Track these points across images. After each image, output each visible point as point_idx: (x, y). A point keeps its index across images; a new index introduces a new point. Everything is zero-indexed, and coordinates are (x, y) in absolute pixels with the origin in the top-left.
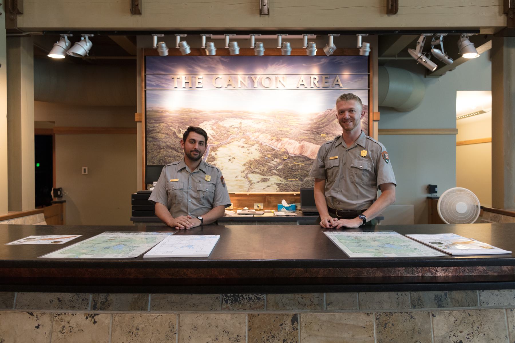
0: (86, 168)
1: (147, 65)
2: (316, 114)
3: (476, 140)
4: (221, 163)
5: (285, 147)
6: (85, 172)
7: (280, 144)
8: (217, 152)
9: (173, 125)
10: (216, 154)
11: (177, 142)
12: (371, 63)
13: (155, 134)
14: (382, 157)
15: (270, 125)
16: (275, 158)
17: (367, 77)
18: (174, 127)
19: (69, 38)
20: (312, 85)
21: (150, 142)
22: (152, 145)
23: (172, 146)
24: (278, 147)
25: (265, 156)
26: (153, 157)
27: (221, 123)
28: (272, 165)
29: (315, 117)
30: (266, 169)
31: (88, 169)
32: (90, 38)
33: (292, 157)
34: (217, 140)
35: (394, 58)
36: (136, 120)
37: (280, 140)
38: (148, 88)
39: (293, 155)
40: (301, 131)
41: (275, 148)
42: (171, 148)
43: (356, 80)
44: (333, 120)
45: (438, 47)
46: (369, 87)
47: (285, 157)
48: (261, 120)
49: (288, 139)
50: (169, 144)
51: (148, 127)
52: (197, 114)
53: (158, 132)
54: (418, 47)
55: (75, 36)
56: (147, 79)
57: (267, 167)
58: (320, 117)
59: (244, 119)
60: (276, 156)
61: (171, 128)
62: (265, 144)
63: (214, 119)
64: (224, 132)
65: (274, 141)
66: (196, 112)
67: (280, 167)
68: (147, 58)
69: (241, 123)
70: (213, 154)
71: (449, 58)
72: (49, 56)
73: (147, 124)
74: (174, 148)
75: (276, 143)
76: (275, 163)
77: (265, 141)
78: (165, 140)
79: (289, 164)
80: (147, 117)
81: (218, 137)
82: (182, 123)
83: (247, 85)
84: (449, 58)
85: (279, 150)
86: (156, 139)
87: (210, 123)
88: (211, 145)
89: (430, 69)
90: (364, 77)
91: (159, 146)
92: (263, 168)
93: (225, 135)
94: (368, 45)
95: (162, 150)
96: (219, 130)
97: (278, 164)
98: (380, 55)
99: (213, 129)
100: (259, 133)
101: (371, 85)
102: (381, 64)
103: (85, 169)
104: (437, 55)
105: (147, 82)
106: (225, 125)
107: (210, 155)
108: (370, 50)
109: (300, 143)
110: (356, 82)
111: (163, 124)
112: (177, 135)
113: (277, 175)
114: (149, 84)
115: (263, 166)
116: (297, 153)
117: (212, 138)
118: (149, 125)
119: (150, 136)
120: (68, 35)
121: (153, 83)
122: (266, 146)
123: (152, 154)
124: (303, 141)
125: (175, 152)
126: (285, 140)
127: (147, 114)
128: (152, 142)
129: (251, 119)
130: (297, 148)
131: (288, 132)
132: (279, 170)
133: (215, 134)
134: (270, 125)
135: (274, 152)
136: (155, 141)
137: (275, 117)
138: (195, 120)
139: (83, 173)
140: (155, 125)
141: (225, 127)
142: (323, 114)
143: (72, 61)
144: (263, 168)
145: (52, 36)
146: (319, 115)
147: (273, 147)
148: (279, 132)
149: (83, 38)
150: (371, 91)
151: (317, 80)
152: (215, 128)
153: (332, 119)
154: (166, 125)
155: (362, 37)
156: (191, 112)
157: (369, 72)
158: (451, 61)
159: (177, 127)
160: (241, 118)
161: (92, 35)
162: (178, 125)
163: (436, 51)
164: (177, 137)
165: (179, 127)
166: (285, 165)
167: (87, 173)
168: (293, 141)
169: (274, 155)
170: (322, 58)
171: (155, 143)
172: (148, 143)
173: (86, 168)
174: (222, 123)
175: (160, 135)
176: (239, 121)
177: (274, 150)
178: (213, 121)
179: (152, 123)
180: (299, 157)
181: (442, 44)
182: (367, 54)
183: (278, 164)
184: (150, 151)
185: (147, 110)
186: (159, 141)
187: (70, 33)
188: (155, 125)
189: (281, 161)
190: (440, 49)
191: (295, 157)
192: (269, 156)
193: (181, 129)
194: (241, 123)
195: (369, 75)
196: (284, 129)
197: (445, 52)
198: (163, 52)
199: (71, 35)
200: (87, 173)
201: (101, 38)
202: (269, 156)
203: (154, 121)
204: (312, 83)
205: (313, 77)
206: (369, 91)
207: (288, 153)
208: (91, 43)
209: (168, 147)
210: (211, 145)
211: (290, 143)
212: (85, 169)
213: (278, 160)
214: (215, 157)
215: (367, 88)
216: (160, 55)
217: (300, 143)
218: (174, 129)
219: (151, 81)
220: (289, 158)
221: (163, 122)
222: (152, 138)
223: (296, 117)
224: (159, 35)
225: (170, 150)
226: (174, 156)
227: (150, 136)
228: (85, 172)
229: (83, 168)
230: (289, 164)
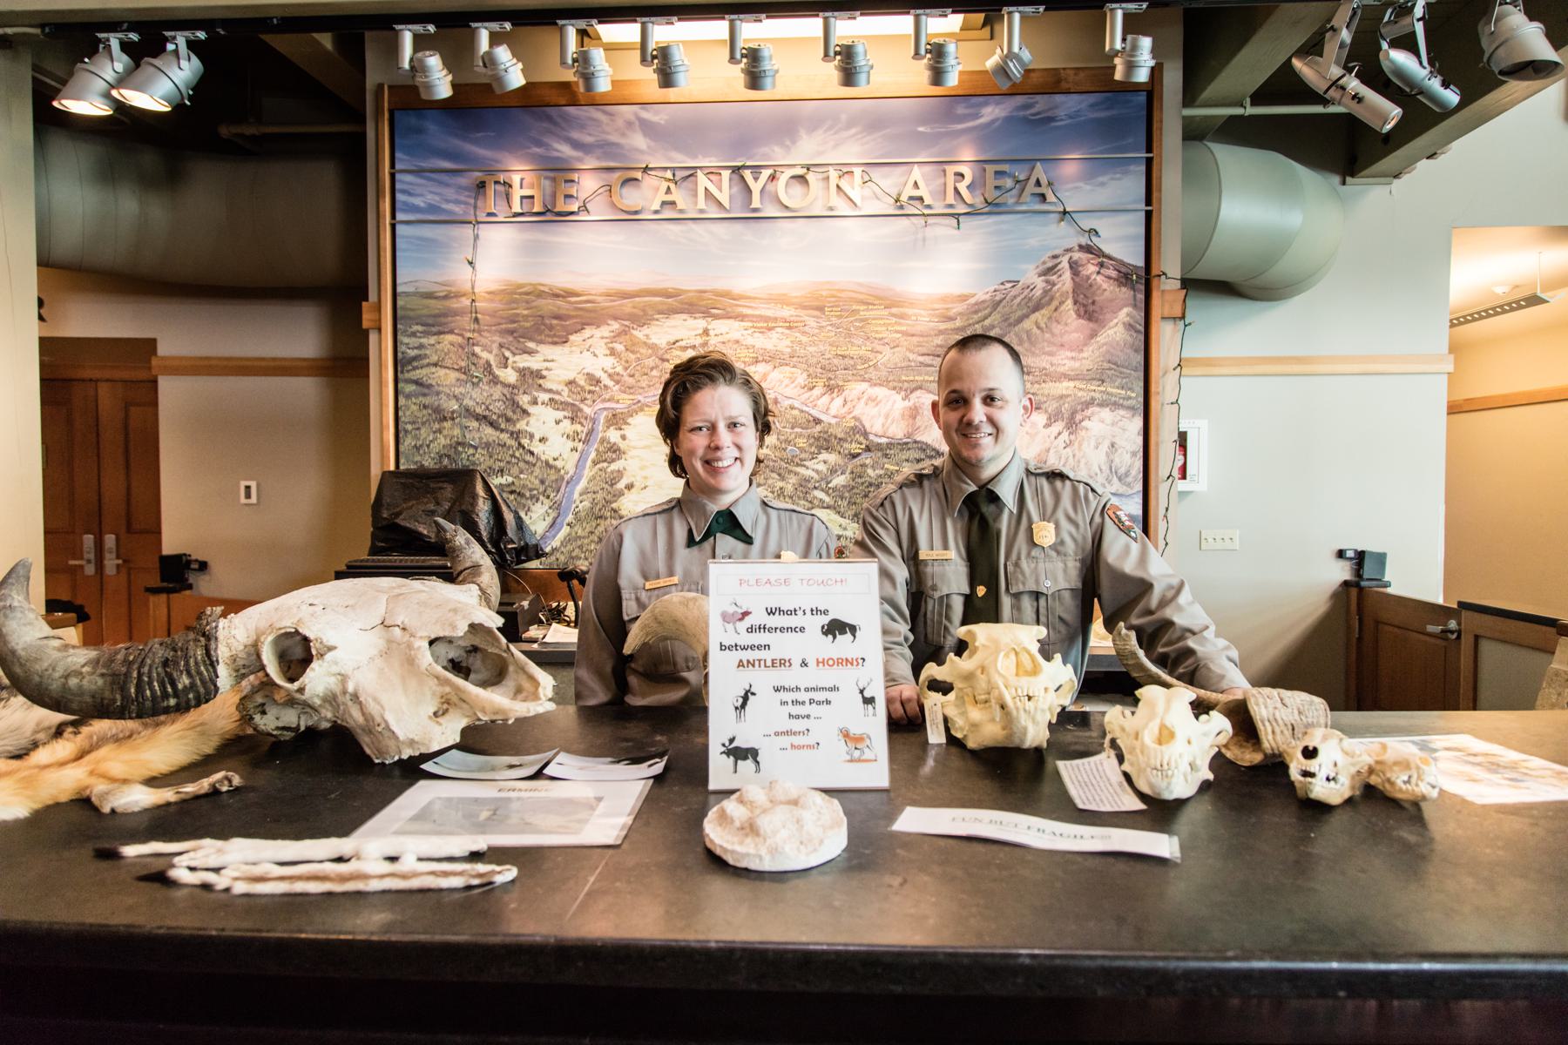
0: (253, 484)
1: (397, 141)
2: (963, 298)
3: (1504, 397)
4: (642, 468)
5: (856, 413)
6: (248, 496)
7: (838, 401)
8: (628, 431)
9: (483, 341)
10: (624, 437)
11: (496, 396)
12: (1155, 125)
13: (424, 371)
14: (1109, 523)
15: (804, 339)
16: (820, 448)
17: (1143, 168)
18: (485, 348)
19: (126, 47)
20: (951, 198)
21: (408, 397)
22: (415, 408)
23: (478, 410)
24: (833, 411)
25: (788, 442)
26: (417, 448)
27: (640, 334)
28: (809, 473)
29: (959, 308)
30: (789, 488)
31: (258, 486)
32: (192, 45)
33: (879, 447)
34: (629, 389)
35: (1238, 111)
36: (365, 325)
37: (840, 389)
38: (400, 216)
39: (883, 440)
40: (912, 356)
41: (823, 417)
42: (478, 418)
43: (1101, 179)
44: (1020, 320)
45: (1407, 42)
46: (1148, 202)
47: (855, 448)
48: (775, 319)
49: (865, 385)
50: (471, 403)
51: (402, 348)
52: (559, 302)
53: (435, 365)
54: (1331, 49)
55: (148, 39)
56: (398, 186)
57: (793, 480)
58: (977, 308)
59: (716, 317)
60: (825, 442)
61: (477, 349)
62: (787, 403)
63: (616, 318)
64: (650, 362)
65: (817, 391)
66: (557, 296)
67: (839, 480)
68: (397, 114)
69: (706, 332)
70: (613, 436)
71: (1445, 85)
72: (55, 104)
73: (400, 337)
74: (485, 417)
75: (826, 399)
76: (822, 467)
77: (789, 392)
78: (457, 391)
79: (870, 471)
80: (400, 313)
81: (631, 380)
82: (511, 332)
83: (727, 205)
84: (1445, 85)
85: (833, 421)
86: (430, 386)
87: (605, 331)
88: (607, 405)
89: (1374, 124)
90: (1132, 168)
91: (437, 410)
92: (781, 484)
93: (655, 373)
94: (1146, 43)
95: (447, 424)
96: (633, 357)
97: (833, 471)
98: (1189, 98)
99: (613, 353)
100: (768, 367)
101: (1155, 195)
102: (1194, 133)
103: (248, 488)
104: (1400, 73)
105: (400, 197)
106: (654, 340)
107: (603, 441)
108: (1152, 63)
109: (906, 398)
110: (1102, 184)
111: (450, 337)
112: (498, 372)
113: (828, 507)
114: (405, 203)
115: (783, 478)
116: (898, 431)
117: (611, 384)
118: (406, 340)
119: (407, 375)
120: (120, 35)
121: (418, 201)
122: (792, 408)
123: (416, 438)
124: (918, 393)
125: (489, 430)
126: (856, 388)
127: (400, 303)
128: (416, 396)
129: (741, 317)
130: (897, 413)
131: (865, 360)
132: (834, 489)
133: (619, 369)
134: (804, 339)
135: (818, 428)
136: (425, 395)
137: (821, 309)
138: (555, 322)
139: (243, 500)
140: (424, 341)
141: (654, 347)
142: (987, 297)
143: (125, 127)
144: (781, 484)
145: (75, 38)
146: (972, 301)
147: (815, 413)
148: (836, 361)
149: (170, 47)
150: (1155, 215)
151: (968, 180)
152: (619, 347)
153: (1019, 313)
154: (460, 339)
155: (1126, 16)
156: (541, 295)
157: (1149, 149)
158: (1452, 97)
159: (495, 346)
160: (706, 313)
161: (201, 35)
162: (497, 339)
163: (1400, 57)
164: (495, 381)
165: (501, 346)
166: (856, 475)
167: (254, 499)
168: (881, 392)
169: (817, 439)
170: (986, 104)
171: (426, 400)
172: (402, 401)
173: (253, 484)
174: (645, 330)
175: (442, 372)
176: (701, 324)
177: (817, 421)
178: (615, 326)
179: (414, 334)
180: (904, 446)
181: (1419, 28)
182: (1142, 76)
183: (833, 471)
184: (409, 427)
185: (399, 289)
186: (438, 393)
187: (129, 30)
188: (424, 341)
189: (841, 462)
190: (1415, 51)
191: (890, 446)
192: (801, 442)
193: (507, 354)
194: (706, 332)
195: (1149, 162)
196: (853, 351)
197: (1431, 63)
198: (429, 87)
199: (134, 37)
200: (254, 499)
201: (230, 47)
202: (801, 442)
203: (420, 328)
204: (950, 191)
205: (951, 169)
206: (1149, 215)
207: (865, 434)
208: (195, 61)
209: (469, 413)
210: (607, 405)
211: (872, 399)
212: (248, 488)
213: (832, 458)
214: (622, 445)
215: (1142, 206)
216: (424, 96)
217: (906, 398)
218: (485, 355)
219: (410, 194)
220: (868, 449)
221: (451, 332)
222: (417, 383)
223: (894, 310)
224: (418, 28)
225: (475, 424)
226: (488, 445)
227: (407, 375)
228: (248, 496)
229: (243, 484)
230: (870, 471)
